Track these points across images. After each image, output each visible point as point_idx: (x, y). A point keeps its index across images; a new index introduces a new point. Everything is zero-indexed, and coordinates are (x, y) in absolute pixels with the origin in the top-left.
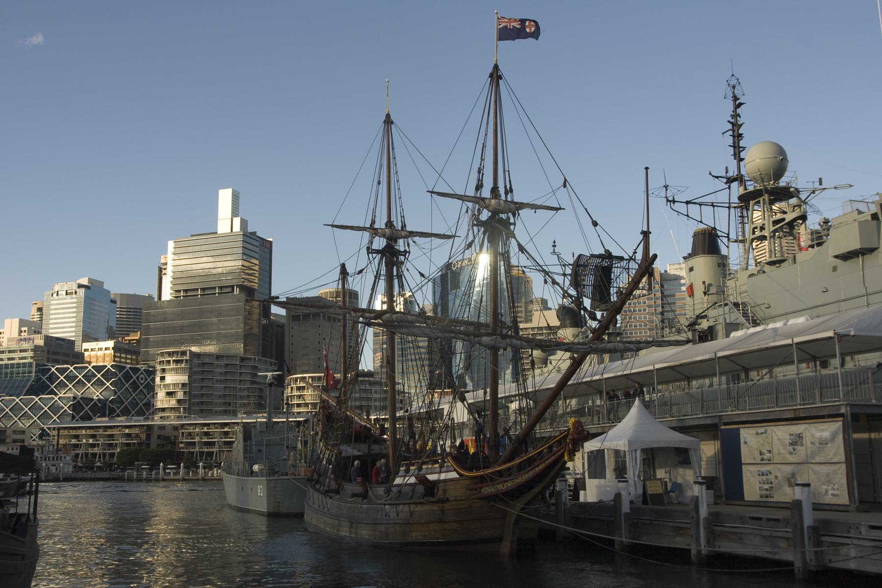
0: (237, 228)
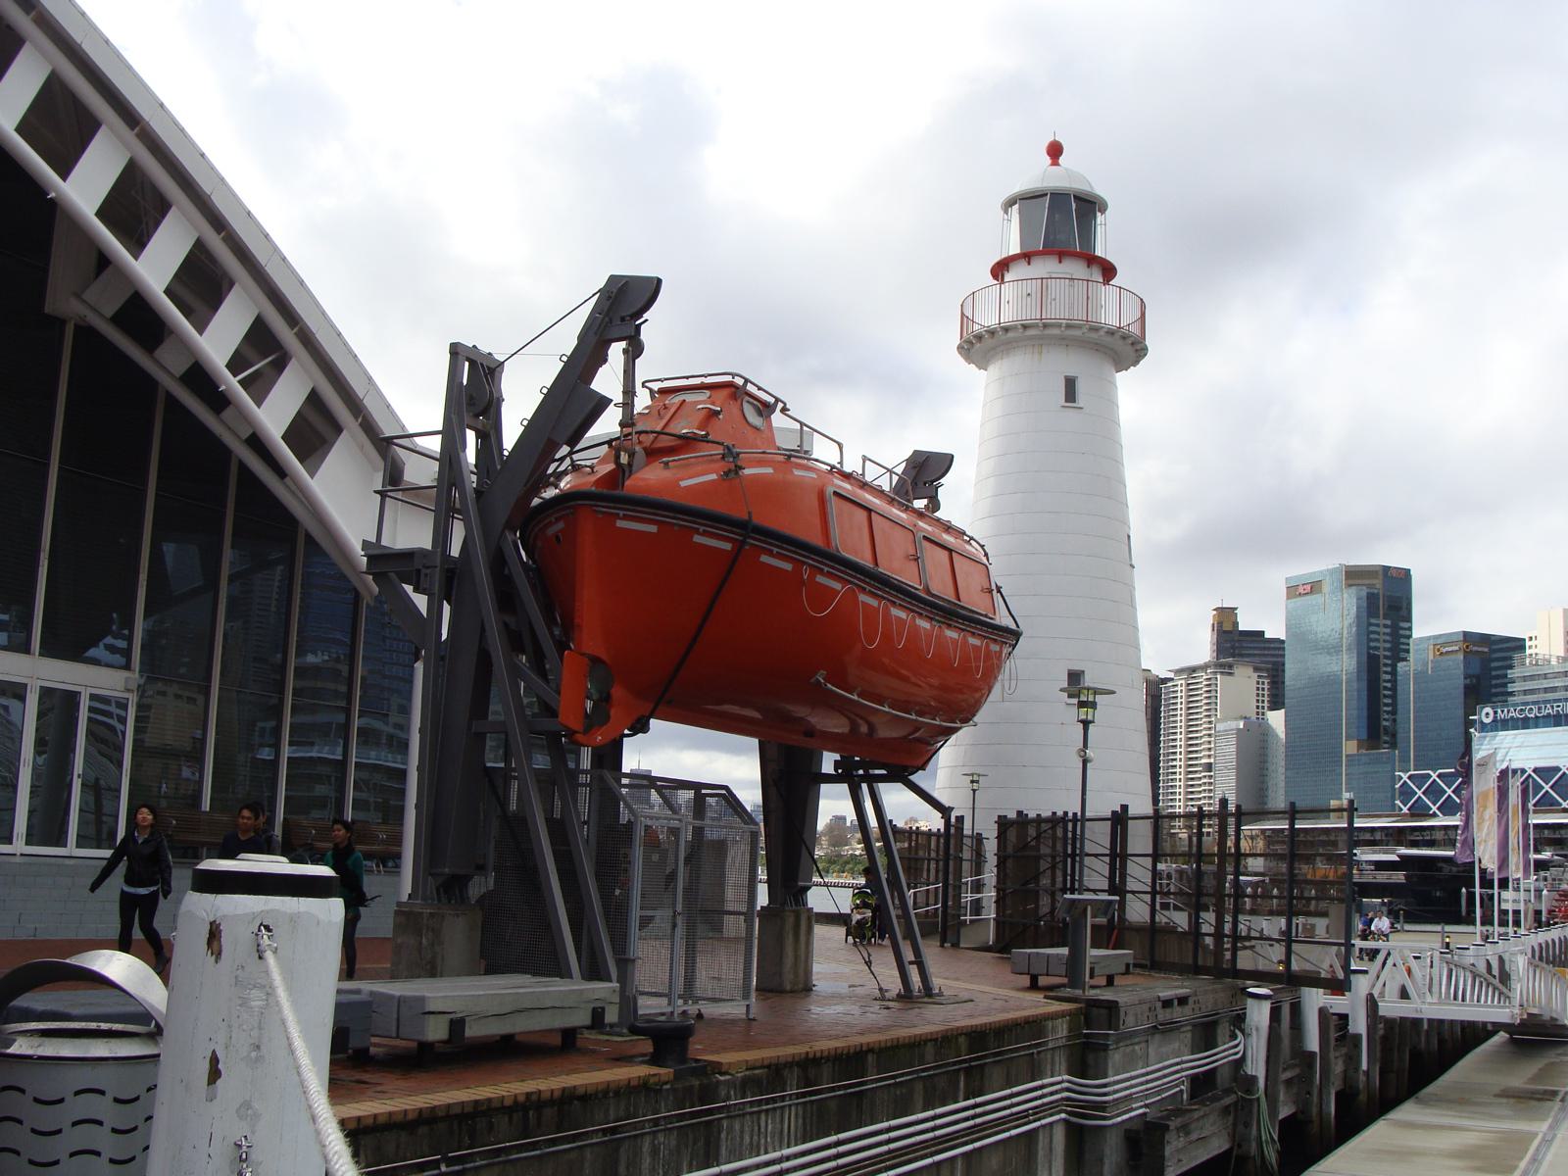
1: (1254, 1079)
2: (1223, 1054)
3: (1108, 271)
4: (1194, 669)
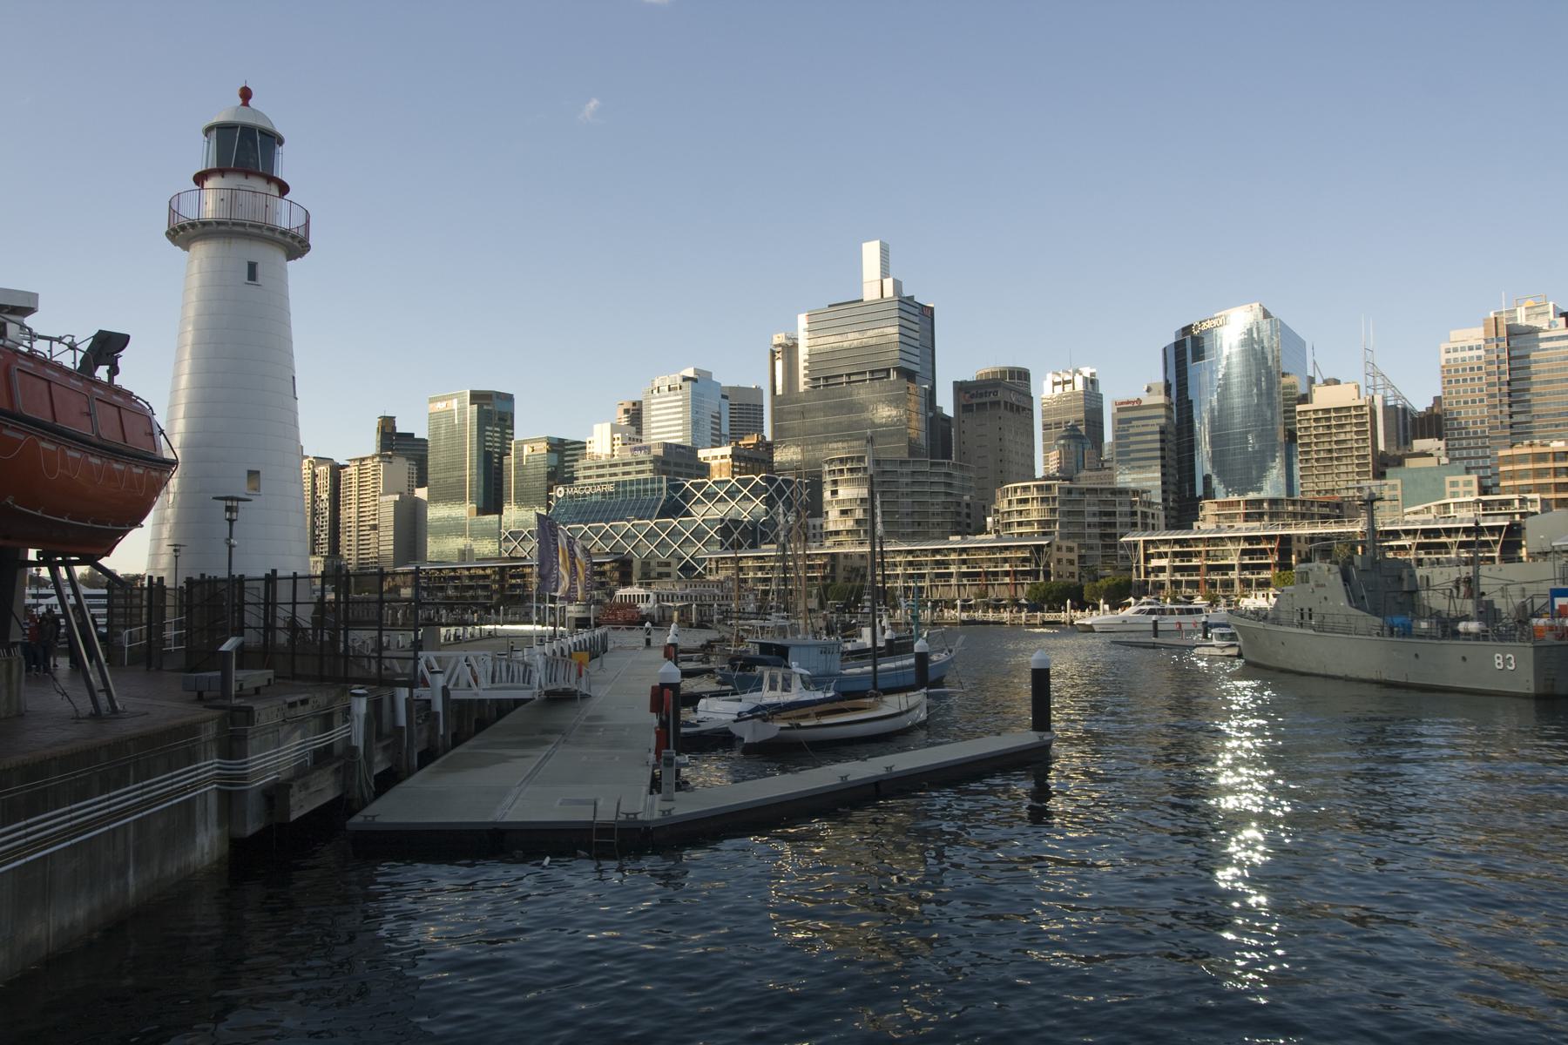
0: (889, 292)
1: (356, 748)
2: (338, 733)
3: (284, 189)
4: (363, 459)
